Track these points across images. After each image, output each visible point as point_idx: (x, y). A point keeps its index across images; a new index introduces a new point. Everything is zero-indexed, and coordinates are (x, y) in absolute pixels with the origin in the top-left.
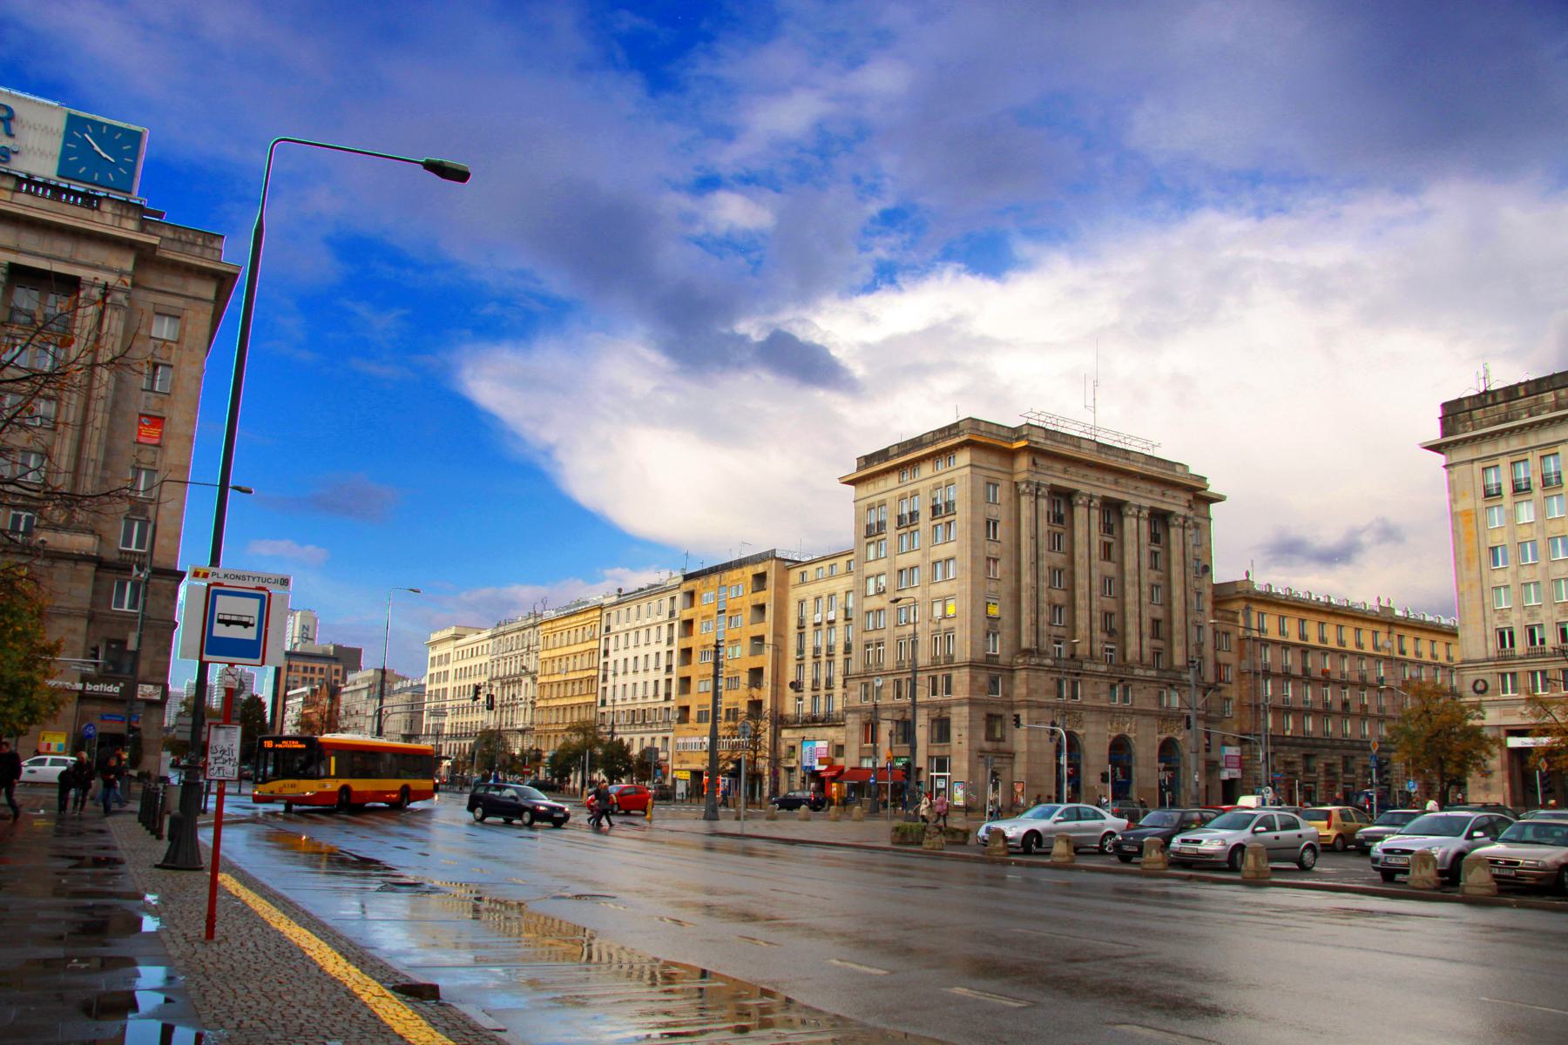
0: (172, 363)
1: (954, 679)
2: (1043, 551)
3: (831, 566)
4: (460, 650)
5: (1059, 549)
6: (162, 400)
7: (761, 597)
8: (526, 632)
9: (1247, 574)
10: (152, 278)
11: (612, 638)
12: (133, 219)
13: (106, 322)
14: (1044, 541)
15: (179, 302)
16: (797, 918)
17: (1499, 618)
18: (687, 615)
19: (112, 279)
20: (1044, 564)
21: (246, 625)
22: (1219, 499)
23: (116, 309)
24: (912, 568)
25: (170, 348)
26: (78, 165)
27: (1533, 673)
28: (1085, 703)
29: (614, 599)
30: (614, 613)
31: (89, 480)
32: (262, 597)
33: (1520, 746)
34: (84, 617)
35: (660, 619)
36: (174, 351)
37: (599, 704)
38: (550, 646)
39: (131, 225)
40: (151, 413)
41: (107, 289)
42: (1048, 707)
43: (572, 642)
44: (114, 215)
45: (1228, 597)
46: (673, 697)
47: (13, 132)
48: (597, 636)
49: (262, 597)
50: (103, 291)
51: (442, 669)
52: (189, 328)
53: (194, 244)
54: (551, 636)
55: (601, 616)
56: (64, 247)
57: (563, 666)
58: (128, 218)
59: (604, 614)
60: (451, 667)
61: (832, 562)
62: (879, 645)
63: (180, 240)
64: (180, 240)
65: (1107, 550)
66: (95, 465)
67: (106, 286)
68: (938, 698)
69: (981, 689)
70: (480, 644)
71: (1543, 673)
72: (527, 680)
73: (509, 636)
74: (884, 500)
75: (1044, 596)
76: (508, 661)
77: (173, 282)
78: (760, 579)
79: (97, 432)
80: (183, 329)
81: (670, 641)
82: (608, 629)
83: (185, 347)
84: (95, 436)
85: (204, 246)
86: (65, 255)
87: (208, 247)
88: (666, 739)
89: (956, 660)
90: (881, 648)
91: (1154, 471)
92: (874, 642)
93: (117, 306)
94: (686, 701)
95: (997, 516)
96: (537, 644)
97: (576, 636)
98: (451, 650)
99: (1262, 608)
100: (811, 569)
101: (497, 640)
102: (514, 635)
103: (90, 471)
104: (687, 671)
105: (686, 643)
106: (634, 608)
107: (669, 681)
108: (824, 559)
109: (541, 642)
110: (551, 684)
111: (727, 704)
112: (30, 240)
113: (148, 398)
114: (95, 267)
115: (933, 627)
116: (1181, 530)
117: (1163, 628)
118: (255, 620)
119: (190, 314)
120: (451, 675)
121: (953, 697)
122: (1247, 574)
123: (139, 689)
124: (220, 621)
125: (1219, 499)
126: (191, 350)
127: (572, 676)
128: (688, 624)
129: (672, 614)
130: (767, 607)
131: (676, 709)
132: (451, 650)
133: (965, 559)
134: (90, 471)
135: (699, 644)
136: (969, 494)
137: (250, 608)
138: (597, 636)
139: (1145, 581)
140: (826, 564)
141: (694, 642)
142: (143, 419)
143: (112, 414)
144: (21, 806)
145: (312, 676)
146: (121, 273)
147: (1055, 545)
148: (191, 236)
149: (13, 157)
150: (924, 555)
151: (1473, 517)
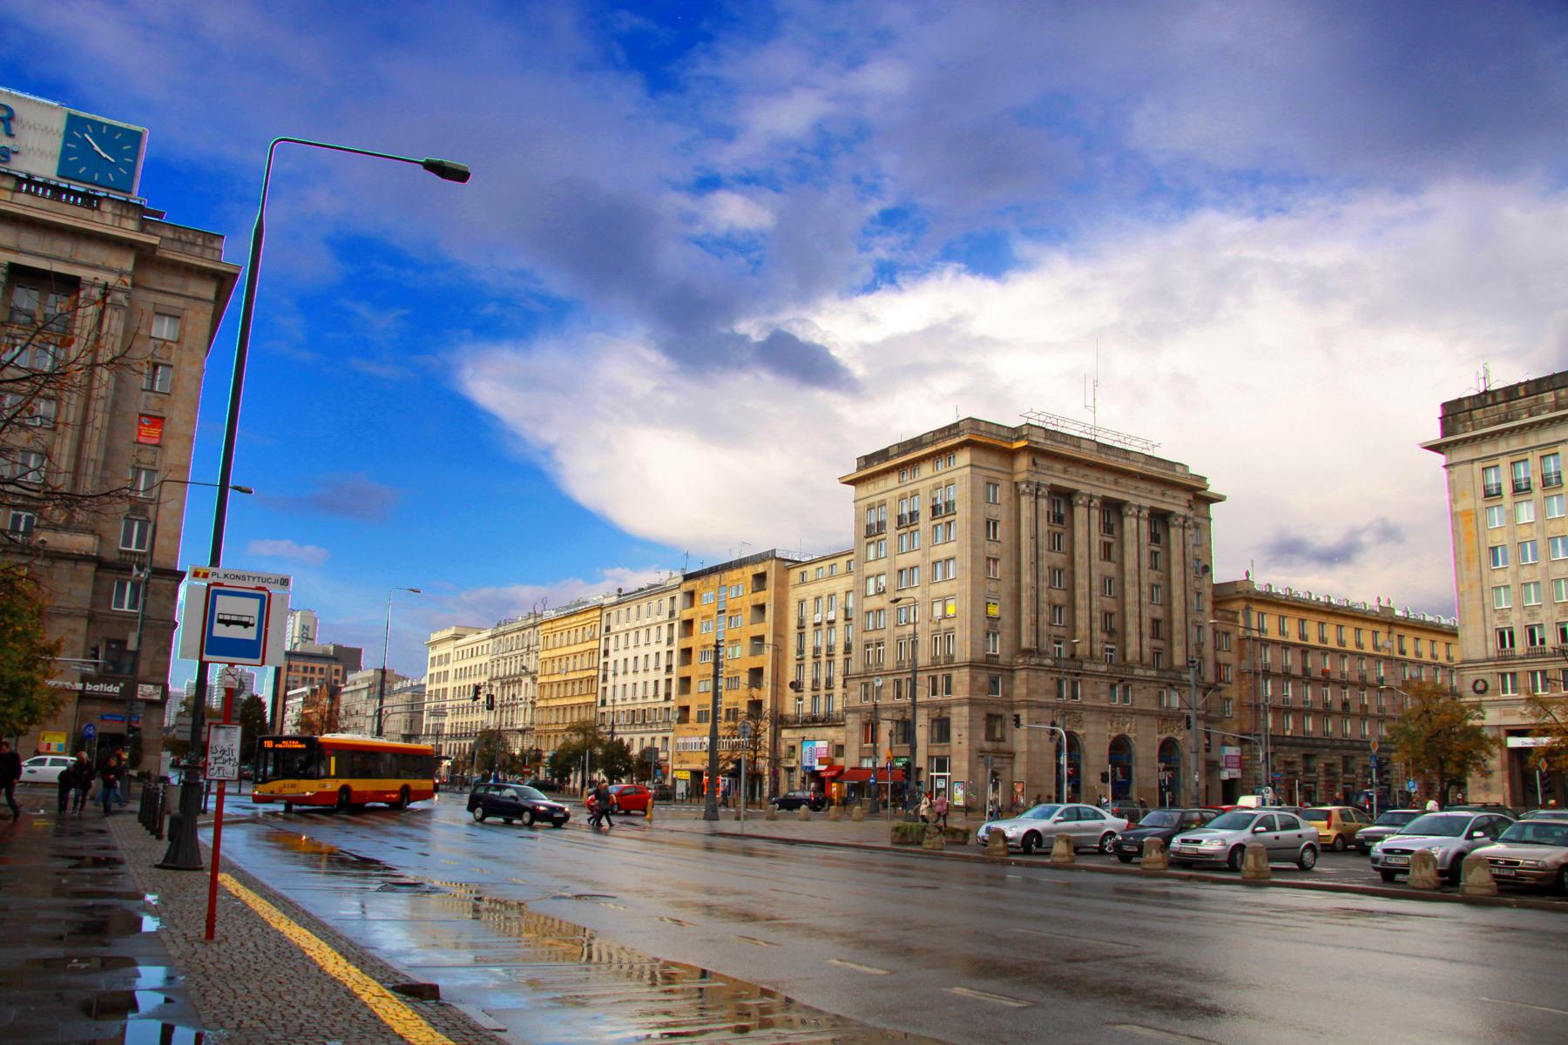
0: (172, 363)
1: (954, 679)
2: (1043, 551)
3: (831, 566)
4: (460, 650)
5: (1059, 549)
6: (162, 400)
7: (761, 597)
8: (526, 632)
9: (1247, 574)
10: (152, 278)
11: (612, 638)
12: (133, 219)
13: (106, 322)
14: (1044, 541)
15: (179, 302)
16: (797, 918)
17: (1499, 618)
18: (687, 615)
19: (112, 279)
20: (1044, 564)
21: (246, 625)
22: (1219, 499)
23: (116, 309)
24: (912, 568)
25: (170, 348)
26: (78, 165)
27: (1533, 673)
28: (1085, 703)
29: (614, 599)
30: (614, 613)
31: (89, 480)
32: (262, 597)
33: (1520, 746)
34: (84, 617)
35: (660, 619)
36: (174, 351)
37: (599, 704)
38: (550, 646)
39: (131, 225)
40: (151, 413)
41: (107, 289)
42: (1048, 707)
43: (572, 642)
44: (114, 215)
45: (1228, 597)
46: (673, 697)
47: (13, 132)
48: (597, 636)
49: (262, 597)
50: (103, 291)
51: (442, 669)
52: (189, 328)
53: (194, 244)
54: (551, 636)
55: (601, 616)
56: (64, 247)
57: (563, 666)
58: (128, 218)
59: (604, 614)
60: (451, 667)
61: (832, 562)
62: (879, 645)
63: (180, 240)
64: (180, 240)
65: (1107, 550)
66: (95, 465)
67: (106, 286)
68: (938, 698)
69: (981, 689)
70: (480, 644)
71: (1543, 673)
72: (527, 680)
73: (509, 636)
74: (884, 500)
75: (1044, 596)
76: (508, 661)
77: (173, 282)
78: (760, 579)
79: (97, 432)
80: (183, 329)
81: (670, 641)
82: (608, 629)
83: (185, 347)
84: (95, 436)
85: (204, 246)
86: (65, 255)
87: (208, 247)
88: (666, 739)
89: (956, 660)
90: (881, 648)
91: (1154, 471)
92: (874, 642)
93: (117, 306)
94: (686, 701)
95: (997, 516)
96: (537, 644)
97: (576, 636)
98: (451, 650)
99: (1262, 608)
100: (811, 569)
101: (497, 640)
102: (514, 635)
103: (90, 471)
104: (687, 671)
105: (686, 643)
106: (634, 608)
107: (669, 681)
108: (824, 559)
109: (541, 642)
110: (551, 684)
111: (727, 704)
112: (30, 240)
113: (148, 398)
114: (95, 267)
115: (933, 627)
116: (1181, 530)
117: (1163, 628)
118: (255, 620)
119: (190, 314)
120: (451, 675)
121: (953, 697)
122: (1247, 574)
123: (139, 689)
124: (220, 621)
125: (1219, 499)
126: (191, 350)
127: (572, 676)
128: (688, 624)
129: (672, 614)
130: (767, 607)
131: (676, 709)
132: (451, 650)
133: (965, 559)
134: (90, 471)
135: (699, 644)
136: (969, 494)
137: (250, 608)
138: (597, 636)
139: (1145, 581)
140: (826, 564)
141: (694, 642)
142: (143, 419)
143: (112, 414)
144: (21, 806)
145: (312, 676)
146: (121, 273)
147: (1055, 545)
148: (191, 236)
149: (13, 157)
150: (924, 555)
151: (1473, 517)
